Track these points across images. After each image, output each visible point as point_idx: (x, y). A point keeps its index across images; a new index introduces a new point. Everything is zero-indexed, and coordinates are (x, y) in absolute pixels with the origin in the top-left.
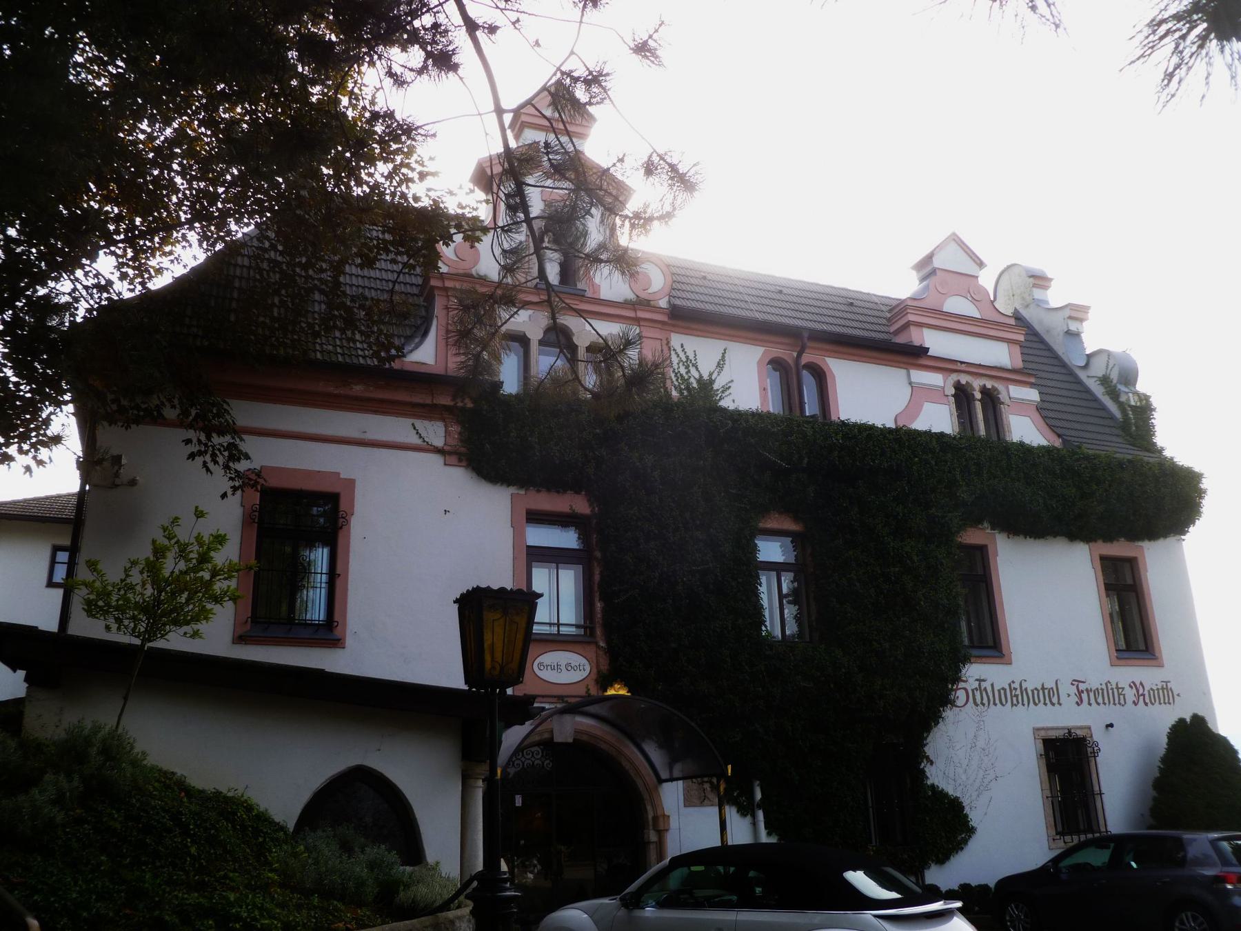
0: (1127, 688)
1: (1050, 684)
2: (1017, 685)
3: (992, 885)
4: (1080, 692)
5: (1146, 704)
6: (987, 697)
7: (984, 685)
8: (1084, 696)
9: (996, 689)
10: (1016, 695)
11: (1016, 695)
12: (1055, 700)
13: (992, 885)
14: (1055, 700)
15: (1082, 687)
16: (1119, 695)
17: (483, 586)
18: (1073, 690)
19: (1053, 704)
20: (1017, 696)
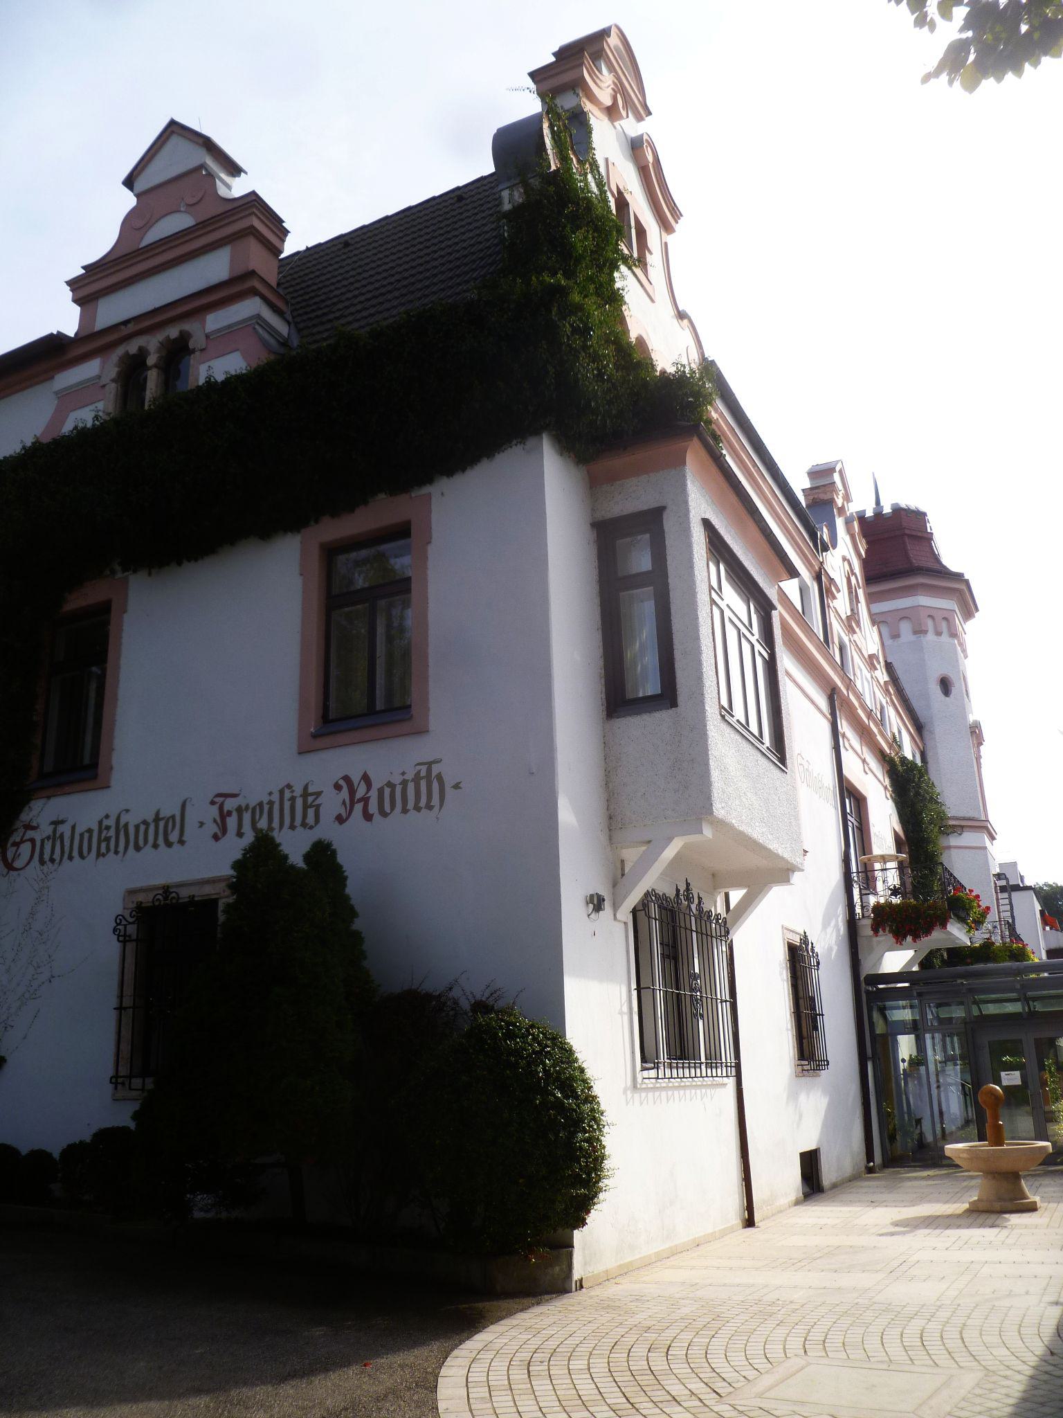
0: (329, 791)
1: (170, 809)
2: (111, 822)
3: (24, 1152)
4: (224, 815)
5: (368, 817)
6: (61, 847)
7: (61, 828)
8: (232, 822)
9: (78, 831)
10: (114, 838)
11: (114, 838)
12: (174, 837)
13: (24, 1152)
14: (174, 837)
15: (230, 804)
16: (306, 807)
17: (913, 508)
18: (214, 811)
19: (169, 844)
20: (108, 839)
